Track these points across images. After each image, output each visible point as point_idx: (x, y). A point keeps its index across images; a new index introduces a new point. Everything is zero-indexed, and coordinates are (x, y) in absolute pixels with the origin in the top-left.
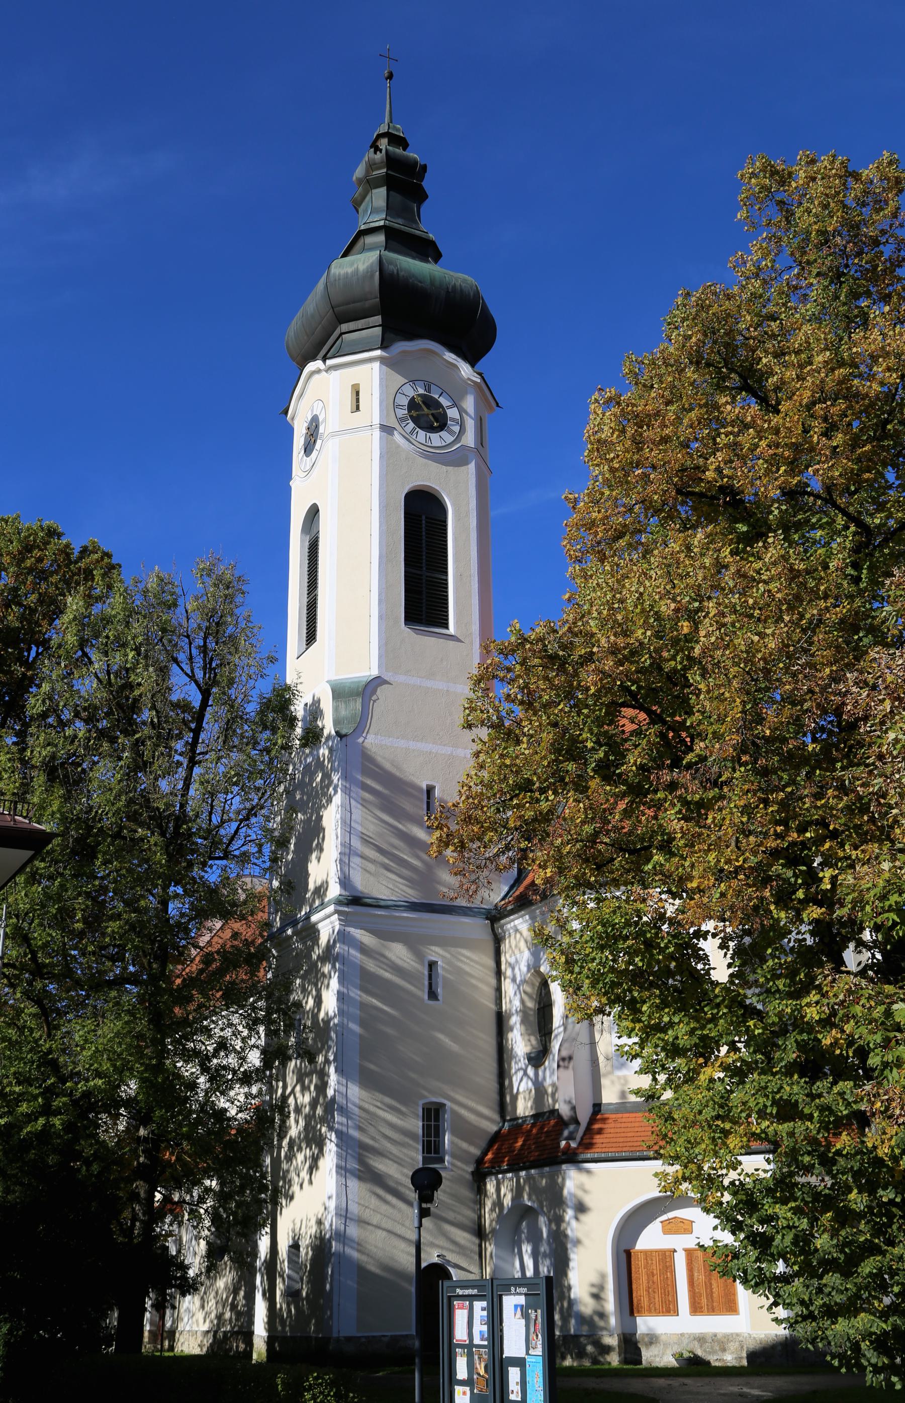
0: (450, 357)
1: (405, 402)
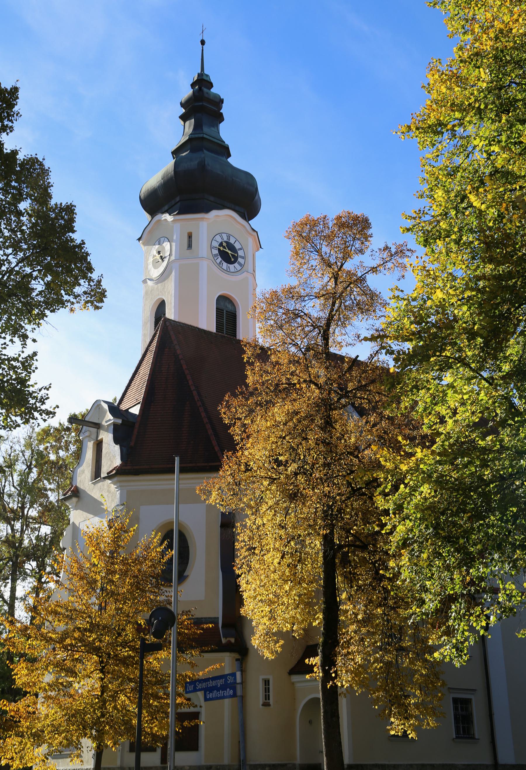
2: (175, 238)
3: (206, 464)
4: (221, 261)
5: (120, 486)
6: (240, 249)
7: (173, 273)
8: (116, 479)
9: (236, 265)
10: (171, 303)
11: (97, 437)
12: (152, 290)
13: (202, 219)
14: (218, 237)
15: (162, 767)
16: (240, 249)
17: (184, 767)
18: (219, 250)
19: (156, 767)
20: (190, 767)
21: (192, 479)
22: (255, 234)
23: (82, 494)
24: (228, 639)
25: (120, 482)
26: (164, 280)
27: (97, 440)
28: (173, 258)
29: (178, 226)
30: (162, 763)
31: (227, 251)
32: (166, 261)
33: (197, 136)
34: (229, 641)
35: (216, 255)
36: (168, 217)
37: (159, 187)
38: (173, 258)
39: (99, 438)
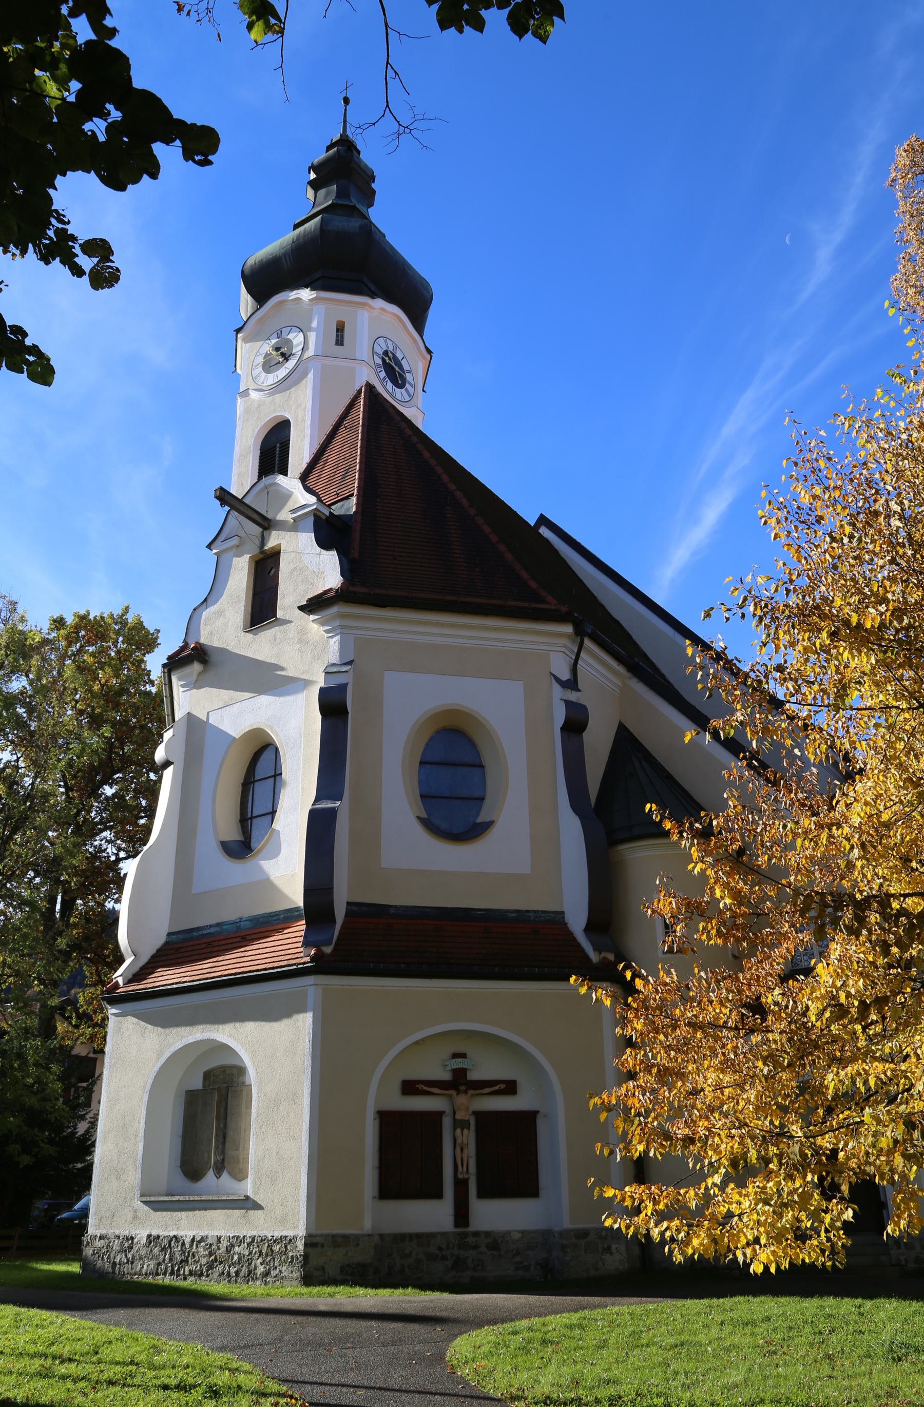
0: (293, 295)
1: (261, 359)
2: (314, 324)
3: (526, 604)
4: (384, 378)
5: (342, 627)
6: (409, 372)
7: (311, 376)
8: (334, 610)
9: (403, 390)
10: (303, 421)
11: (263, 542)
12: (259, 406)
13: (364, 304)
14: (381, 340)
15: (459, 1234)
16: (409, 372)
17: (509, 1233)
18: (383, 360)
19: (444, 1234)
20: (523, 1232)
21: (496, 629)
22: (429, 357)
23: (213, 658)
24: (604, 954)
25: (343, 616)
26: (289, 388)
27: (262, 552)
28: (310, 352)
29: (321, 308)
30: (457, 1225)
31: (393, 365)
32: (292, 363)
33: (339, 202)
34: (605, 958)
35: (378, 365)
36: (306, 294)
37: (285, 254)
38: (310, 352)
39: (271, 544)
